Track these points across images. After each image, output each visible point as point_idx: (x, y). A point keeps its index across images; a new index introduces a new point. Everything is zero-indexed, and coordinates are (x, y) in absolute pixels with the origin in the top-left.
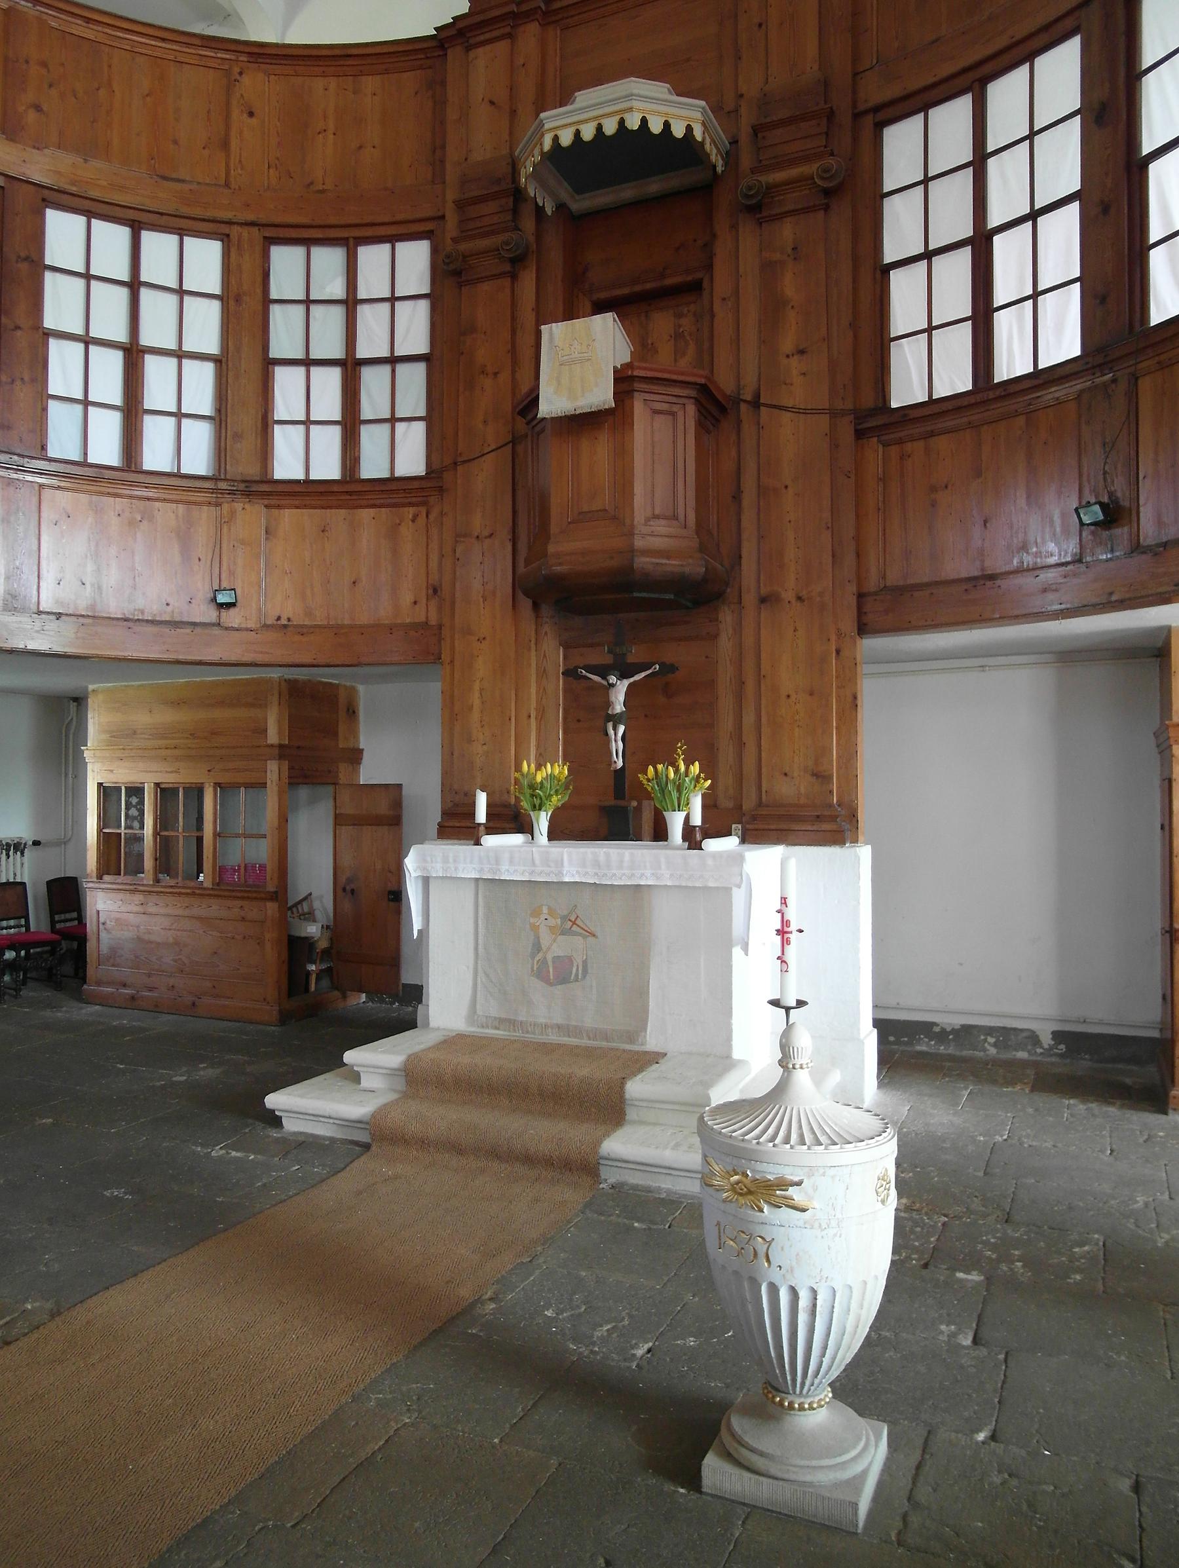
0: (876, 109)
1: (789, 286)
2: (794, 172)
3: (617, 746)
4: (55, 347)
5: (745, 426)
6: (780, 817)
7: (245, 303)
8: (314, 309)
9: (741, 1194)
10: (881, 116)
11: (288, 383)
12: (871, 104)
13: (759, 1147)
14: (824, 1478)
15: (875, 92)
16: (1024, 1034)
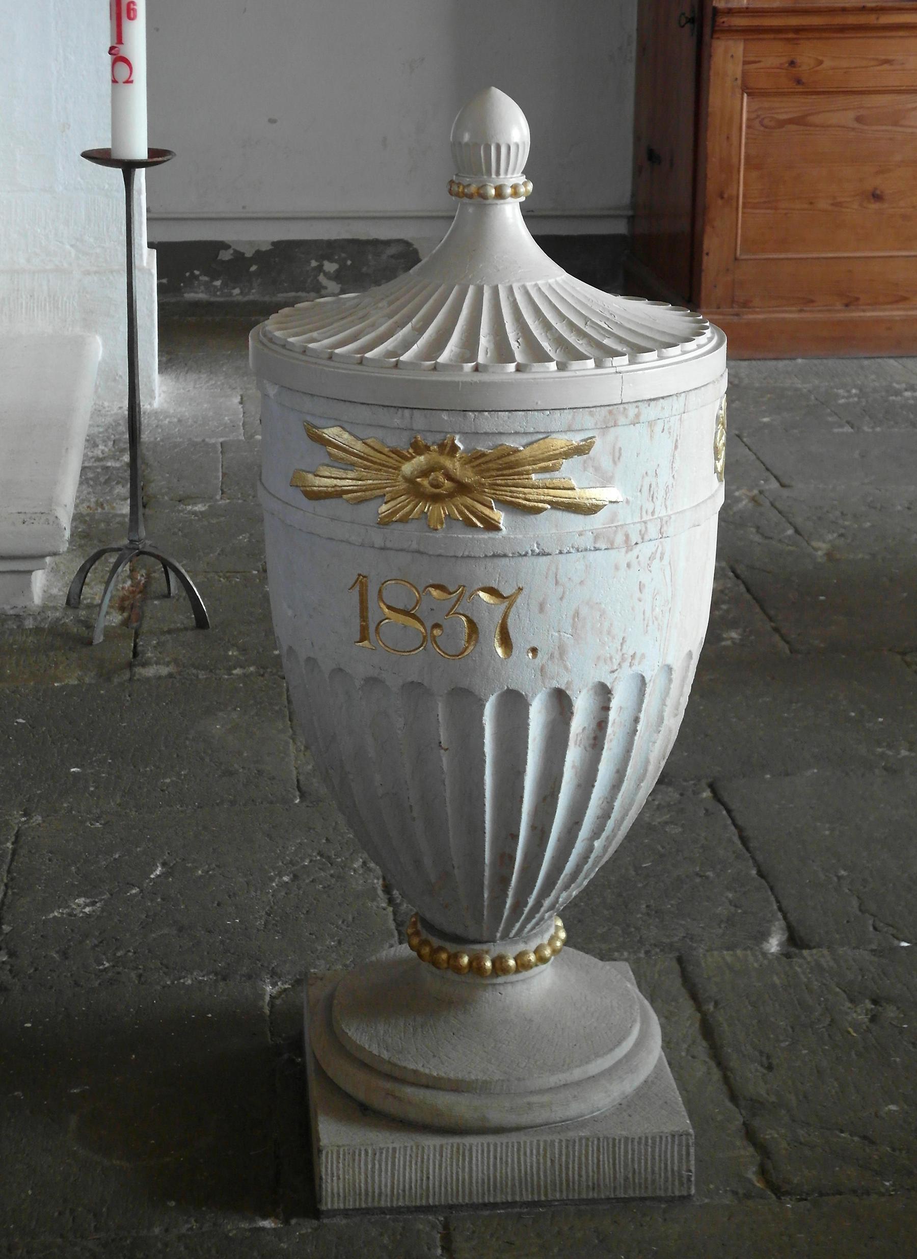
9: (435, 499)
13: (478, 377)
14: (603, 1099)
16: (392, 250)
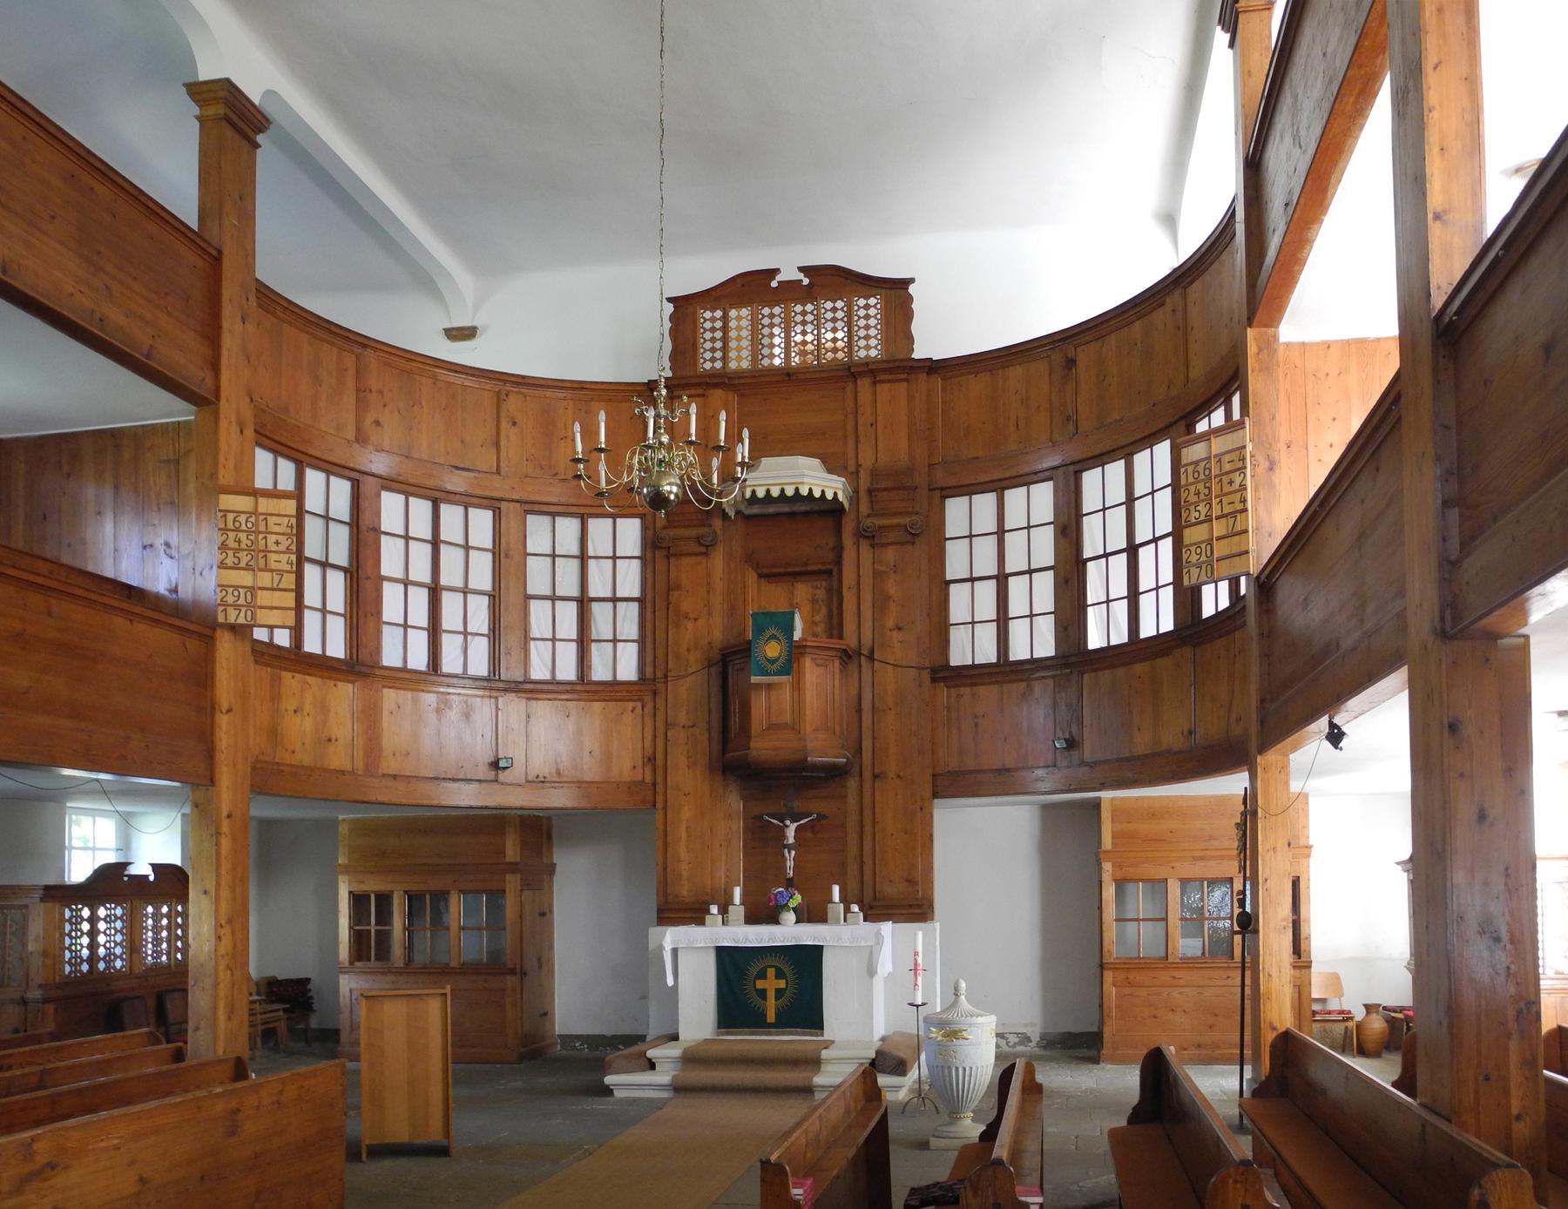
0: (942, 489)
1: (892, 588)
2: (896, 521)
3: (790, 864)
4: (386, 586)
5: (864, 670)
6: (887, 907)
7: (507, 558)
8: (549, 560)
10: (945, 493)
11: (539, 614)
12: (940, 485)
15: (941, 479)
